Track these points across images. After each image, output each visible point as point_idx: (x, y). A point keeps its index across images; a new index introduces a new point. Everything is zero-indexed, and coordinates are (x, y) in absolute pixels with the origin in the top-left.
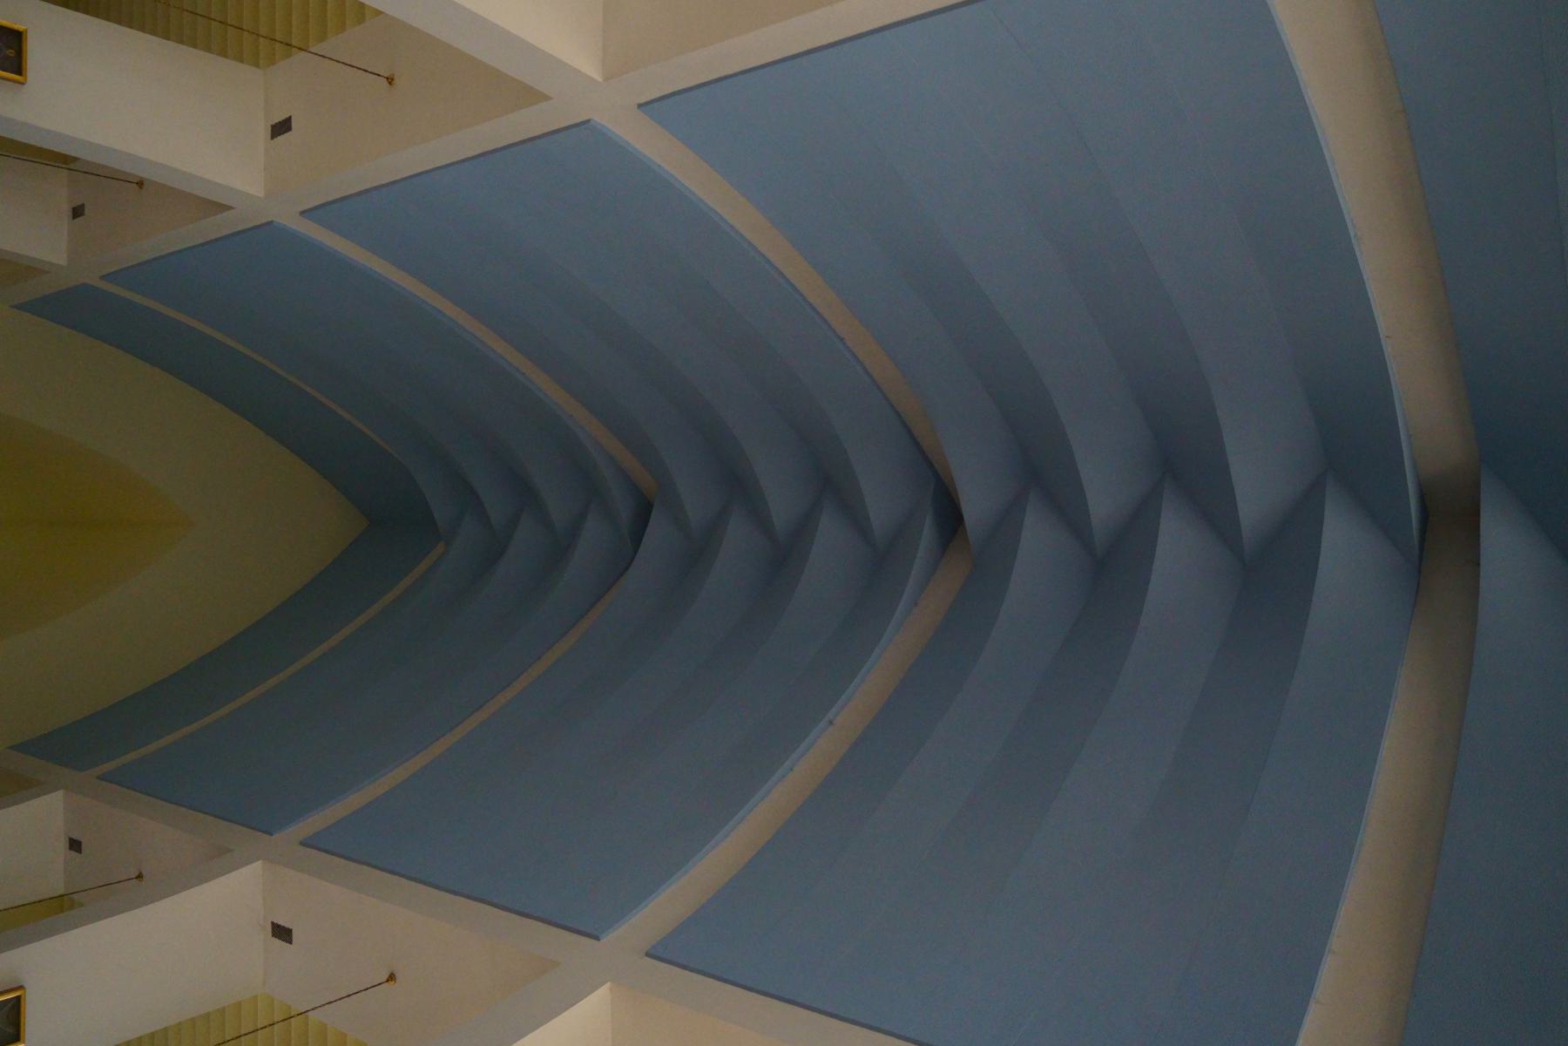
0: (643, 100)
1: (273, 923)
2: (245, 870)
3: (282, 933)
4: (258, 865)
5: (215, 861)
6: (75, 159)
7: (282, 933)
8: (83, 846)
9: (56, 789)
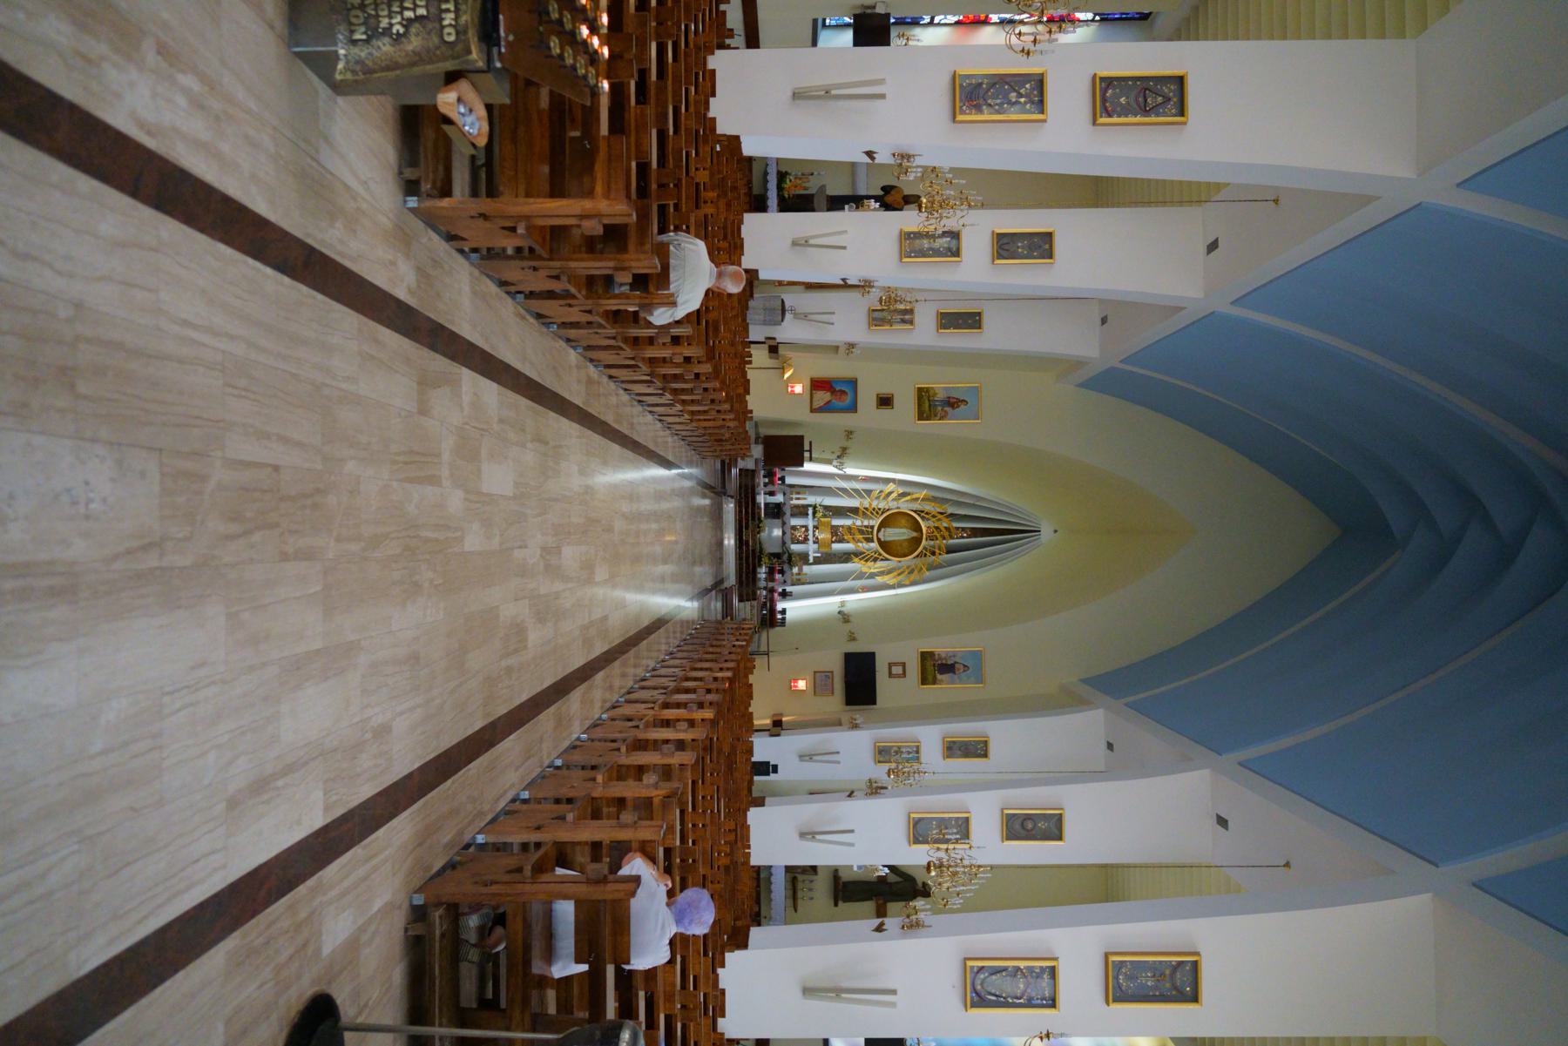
0: (1459, 181)
1: (1217, 815)
2: (1196, 773)
3: (1222, 822)
4: (1206, 772)
5: (1184, 764)
6: (1218, 187)
7: (1222, 822)
8: (1229, 823)
9: (1098, 708)
